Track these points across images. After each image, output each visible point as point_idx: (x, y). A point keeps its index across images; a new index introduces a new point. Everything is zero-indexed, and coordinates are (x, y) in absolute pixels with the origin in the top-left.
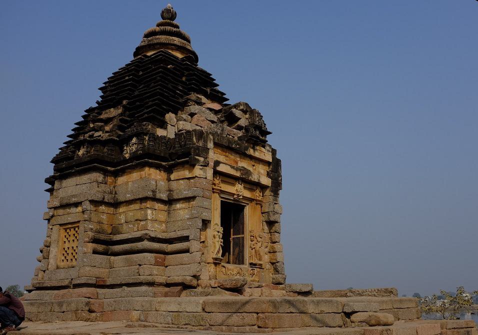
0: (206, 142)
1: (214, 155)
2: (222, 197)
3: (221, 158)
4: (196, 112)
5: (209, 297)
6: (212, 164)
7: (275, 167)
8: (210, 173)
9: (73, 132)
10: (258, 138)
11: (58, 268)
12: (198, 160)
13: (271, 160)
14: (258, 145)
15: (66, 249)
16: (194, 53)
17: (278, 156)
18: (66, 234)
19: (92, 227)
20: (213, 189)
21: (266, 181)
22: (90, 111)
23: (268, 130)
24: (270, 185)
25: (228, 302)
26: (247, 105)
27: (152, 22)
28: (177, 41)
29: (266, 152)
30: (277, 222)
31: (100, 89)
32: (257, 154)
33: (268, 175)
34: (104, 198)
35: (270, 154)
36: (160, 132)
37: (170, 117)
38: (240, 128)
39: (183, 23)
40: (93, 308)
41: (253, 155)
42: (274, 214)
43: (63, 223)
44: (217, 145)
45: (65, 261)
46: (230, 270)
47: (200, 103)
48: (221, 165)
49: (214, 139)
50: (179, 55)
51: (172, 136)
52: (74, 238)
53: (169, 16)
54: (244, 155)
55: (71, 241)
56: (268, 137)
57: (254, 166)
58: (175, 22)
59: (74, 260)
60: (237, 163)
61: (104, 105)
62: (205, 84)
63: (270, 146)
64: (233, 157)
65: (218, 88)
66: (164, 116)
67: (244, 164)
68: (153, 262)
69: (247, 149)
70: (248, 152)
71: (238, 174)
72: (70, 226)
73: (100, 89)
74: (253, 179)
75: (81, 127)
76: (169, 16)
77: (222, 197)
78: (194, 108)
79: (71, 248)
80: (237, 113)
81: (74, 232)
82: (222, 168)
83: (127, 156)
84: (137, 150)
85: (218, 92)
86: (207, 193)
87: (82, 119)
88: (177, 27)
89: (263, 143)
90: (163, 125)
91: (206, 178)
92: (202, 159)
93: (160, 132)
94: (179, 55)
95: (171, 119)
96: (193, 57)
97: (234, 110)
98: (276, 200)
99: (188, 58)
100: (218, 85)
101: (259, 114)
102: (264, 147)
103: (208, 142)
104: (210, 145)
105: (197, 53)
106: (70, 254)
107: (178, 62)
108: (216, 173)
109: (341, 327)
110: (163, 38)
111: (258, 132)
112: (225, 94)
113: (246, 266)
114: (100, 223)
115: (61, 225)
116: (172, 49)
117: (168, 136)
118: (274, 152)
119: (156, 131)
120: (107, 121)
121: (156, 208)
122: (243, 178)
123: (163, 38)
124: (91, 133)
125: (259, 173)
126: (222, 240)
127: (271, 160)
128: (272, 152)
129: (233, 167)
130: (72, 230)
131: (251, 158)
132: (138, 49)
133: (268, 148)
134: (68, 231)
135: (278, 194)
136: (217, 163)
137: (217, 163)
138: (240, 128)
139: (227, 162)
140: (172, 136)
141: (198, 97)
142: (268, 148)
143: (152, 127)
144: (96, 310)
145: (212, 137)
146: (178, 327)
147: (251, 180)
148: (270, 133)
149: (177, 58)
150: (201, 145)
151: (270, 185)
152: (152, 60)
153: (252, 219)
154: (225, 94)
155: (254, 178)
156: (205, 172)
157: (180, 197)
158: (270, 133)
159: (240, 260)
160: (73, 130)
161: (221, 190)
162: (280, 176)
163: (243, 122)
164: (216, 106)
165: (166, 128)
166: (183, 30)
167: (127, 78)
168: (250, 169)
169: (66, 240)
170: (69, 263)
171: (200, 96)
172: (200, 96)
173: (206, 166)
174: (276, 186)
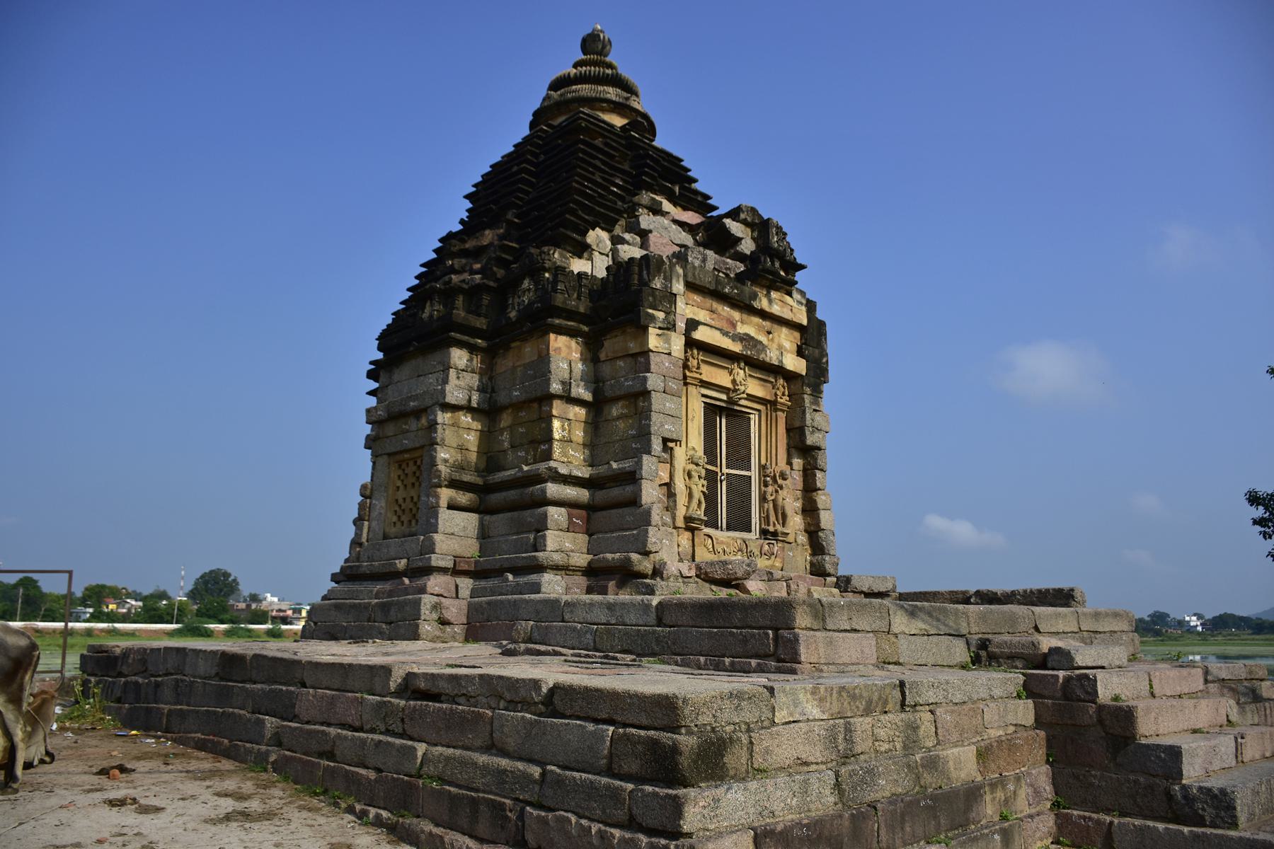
0: (668, 279)
1: (687, 307)
2: (703, 396)
3: (702, 316)
4: (651, 227)
5: (469, 753)
6: (681, 325)
7: (812, 337)
8: (677, 344)
9: (417, 282)
10: (776, 274)
11: (385, 537)
12: (653, 318)
13: (805, 322)
14: (777, 289)
15: (401, 501)
16: (645, 116)
17: (820, 315)
18: (400, 472)
19: (447, 456)
20: (685, 377)
21: (794, 363)
22: (447, 239)
23: (799, 261)
24: (804, 373)
25: (1264, 622)
26: (753, 210)
27: (566, 60)
28: (612, 93)
29: (795, 304)
30: (819, 449)
31: (466, 197)
32: (776, 309)
33: (800, 353)
34: (470, 400)
35: (804, 308)
36: (578, 266)
37: (598, 237)
38: (740, 257)
39: (621, 60)
40: (448, 615)
41: (767, 309)
42: (813, 432)
43: (394, 450)
44: (691, 286)
45: (399, 524)
46: (722, 543)
47: (656, 210)
48: (700, 328)
49: (685, 276)
50: (618, 121)
51: (601, 273)
52: (413, 480)
53: (593, 44)
54: (749, 309)
55: (409, 486)
56: (799, 276)
57: (769, 333)
58: (608, 59)
59: (413, 522)
60: (734, 326)
61: (471, 225)
62: (672, 178)
63: (802, 293)
64: (725, 310)
65: (694, 186)
66: (585, 233)
67: (750, 327)
68: (565, 525)
69: (755, 296)
70: (756, 304)
71: (736, 347)
72: (406, 456)
73: (466, 197)
74: (768, 360)
75: (432, 271)
76: (593, 44)
77: (703, 396)
78: (646, 220)
79: (408, 500)
80: (735, 228)
81: (414, 468)
82: (701, 334)
83: (513, 314)
84: (531, 303)
85: (697, 192)
86: (673, 385)
87: (435, 256)
88: (610, 66)
89: (787, 286)
90: (582, 250)
91: (669, 354)
92: (661, 315)
93: (578, 266)
94: (618, 121)
95: (599, 241)
96: (643, 125)
97: (727, 221)
98: (818, 404)
99: (633, 125)
100: (695, 181)
101: (779, 228)
102: (790, 294)
103: (674, 281)
104: (678, 287)
105: (653, 118)
106: (407, 511)
107: (615, 134)
108: (690, 344)
109: (963, 667)
110: (585, 90)
111: (777, 264)
112: (709, 198)
113: (754, 535)
114: (462, 448)
115: (389, 455)
116: (603, 110)
117: (650, 528)
118: (811, 306)
119: (569, 264)
120: (477, 253)
121: (571, 416)
122: (746, 356)
123: (585, 90)
124: (446, 278)
125: (780, 347)
126: (705, 483)
127: (805, 322)
128: (806, 305)
129: (726, 334)
130: (411, 463)
131: (764, 315)
132: (536, 114)
133: (796, 296)
134: (404, 466)
135: (821, 392)
136: (692, 324)
137: (692, 324)
138: (740, 257)
139: (713, 323)
140: (601, 273)
141: (653, 199)
142: (796, 296)
143: (561, 255)
144: (452, 620)
145: (680, 271)
146: (606, 657)
147: (764, 362)
148: (802, 267)
149: (612, 126)
150: (658, 286)
151: (804, 373)
152: (562, 131)
153: (766, 442)
154: (709, 198)
155: (772, 356)
156: (668, 341)
157: (618, 393)
158: (802, 267)
159: (739, 522)
160: (416, 278)
161: (701, 381)
162: (824, 354)
163: (747, 246)
164: (692, 218)
165: (590, 259)
166: (625, 71)
167: (515, 168)
168: (763, 338)
169: (399, 483)
170: (405, 529)
171: (658, 198)
172: (658, 198)
173: (668, 329)
174: (818, 373)
